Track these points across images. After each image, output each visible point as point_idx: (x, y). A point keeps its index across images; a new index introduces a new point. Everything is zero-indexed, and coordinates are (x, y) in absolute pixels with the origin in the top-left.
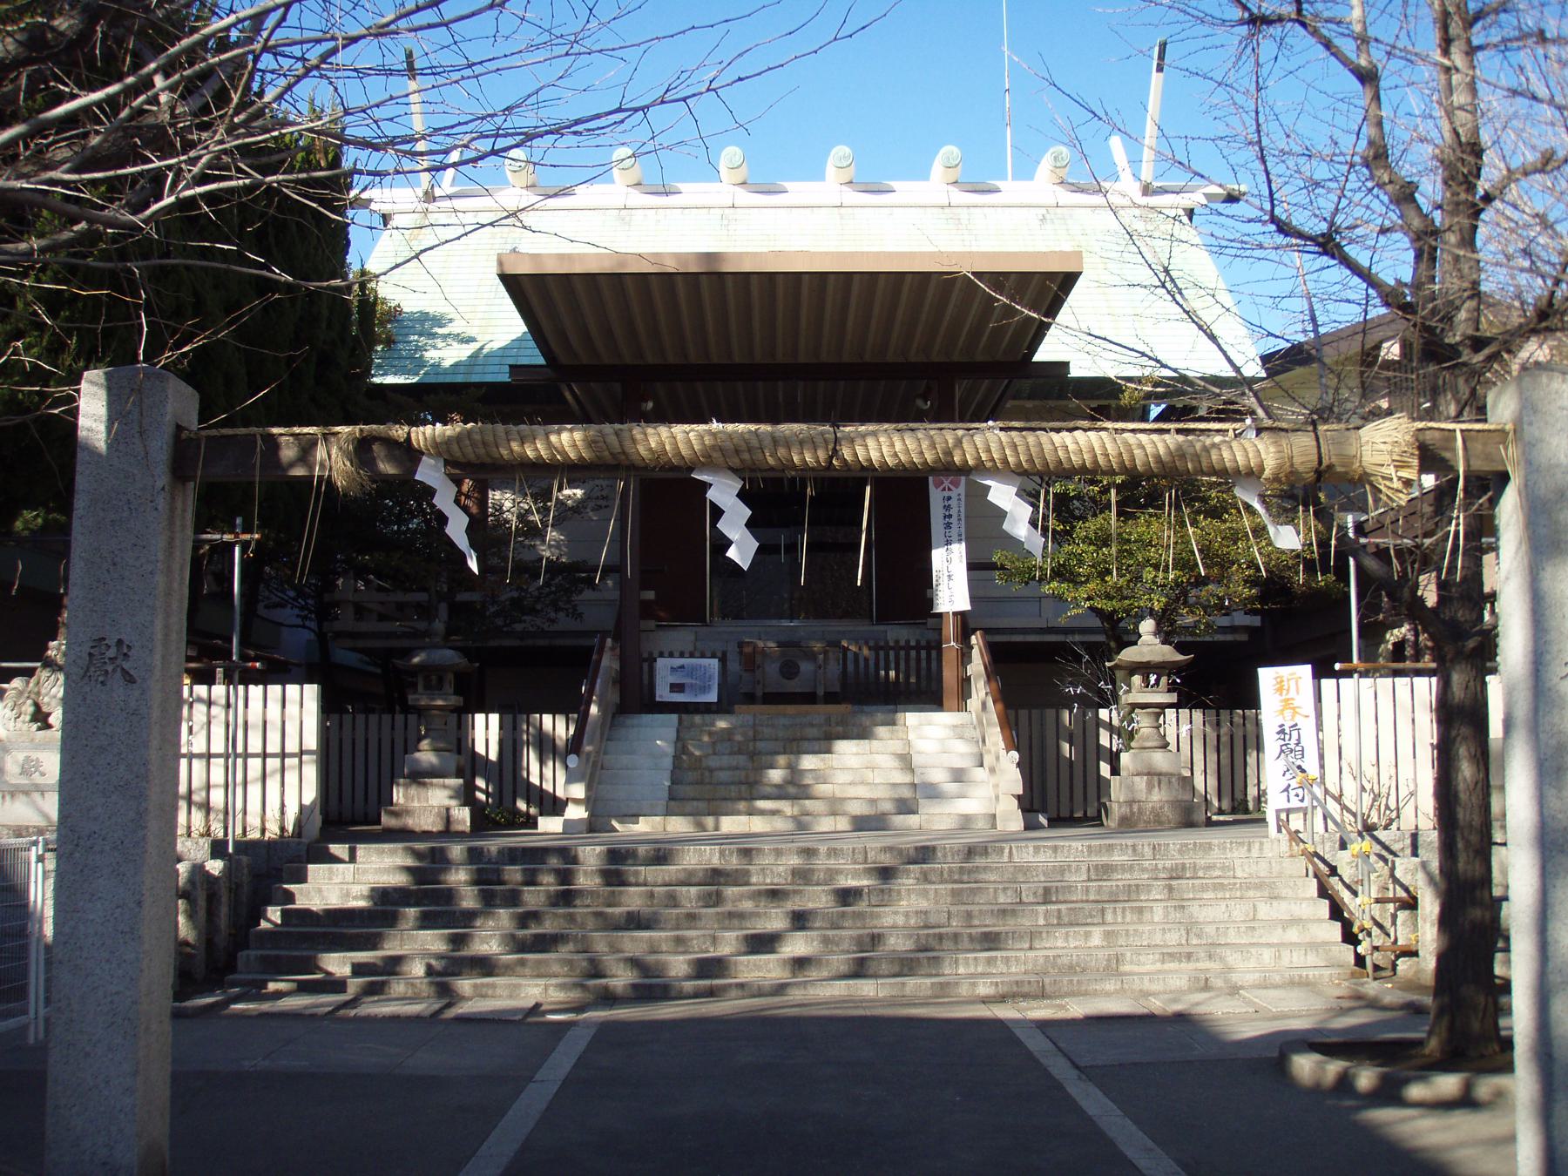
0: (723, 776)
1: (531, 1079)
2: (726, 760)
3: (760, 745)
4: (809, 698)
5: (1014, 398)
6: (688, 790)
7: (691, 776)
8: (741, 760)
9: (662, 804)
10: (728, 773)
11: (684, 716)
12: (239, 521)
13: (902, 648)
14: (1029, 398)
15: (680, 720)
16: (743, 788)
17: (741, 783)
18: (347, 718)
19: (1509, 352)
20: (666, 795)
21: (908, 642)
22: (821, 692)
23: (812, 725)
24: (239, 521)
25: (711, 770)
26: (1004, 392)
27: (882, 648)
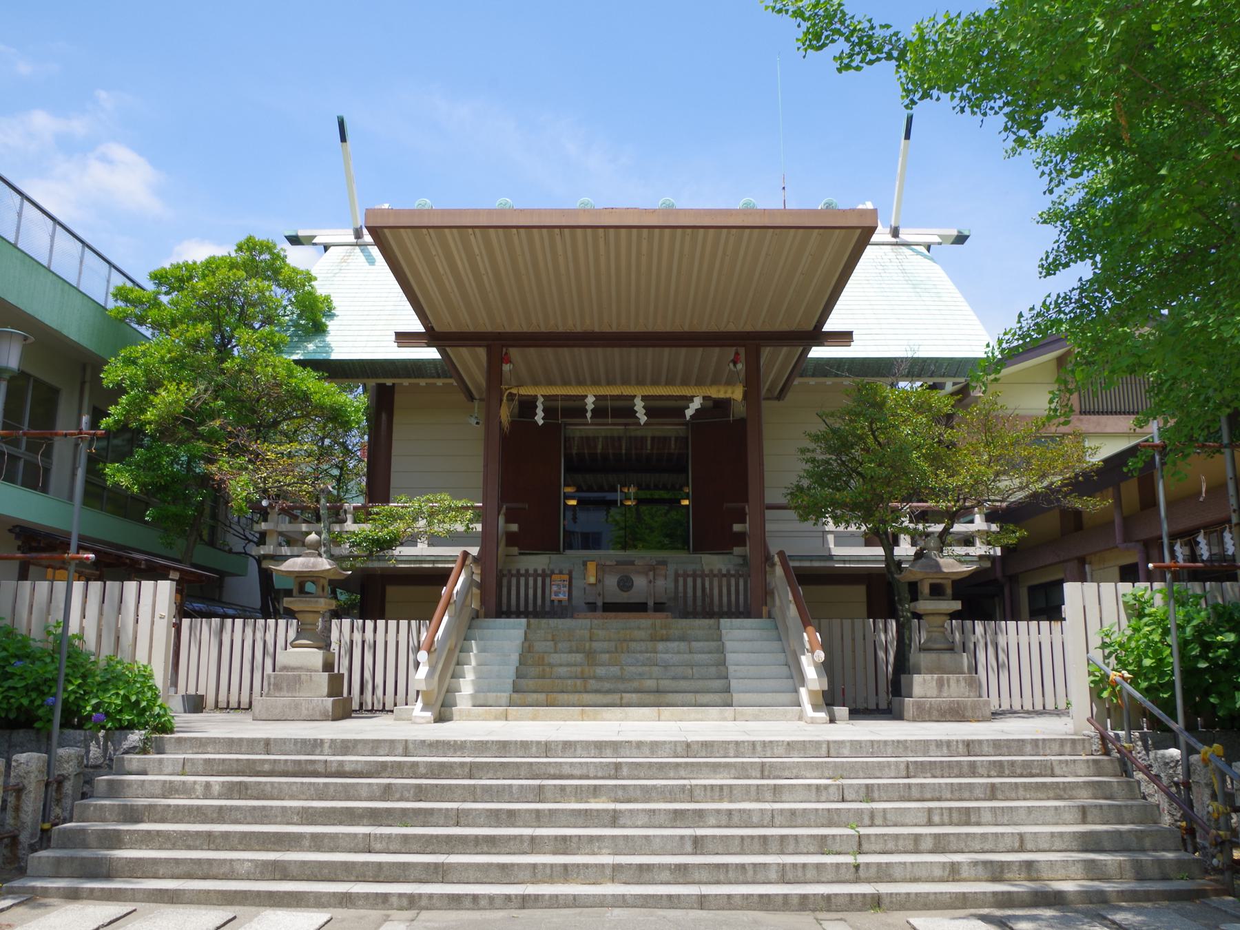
0: (563, 671)
1: (104, 308)
2: (565, 657)
3: (596, 645)
4: (639, 608)
5: (801, 376)
6: (531, 683)
7: (533, 671)
8: (579, 657)
9: (504, 697)
10: (565, 669)
11: (532, 621)
12: (539, 418)
13: (724, 575)
14: (813, 375)
15: (528, 625)
16: (579, 682)
17: (577, 678)
18: (106, 650)
19: (198, 341)
20: (510, 687)
21: (728, 571)
22: (651, 603)
23: (639, 628)
24: (539, 418)
25: (551, 666)
26: (792, 371)
27: (707, 576)
